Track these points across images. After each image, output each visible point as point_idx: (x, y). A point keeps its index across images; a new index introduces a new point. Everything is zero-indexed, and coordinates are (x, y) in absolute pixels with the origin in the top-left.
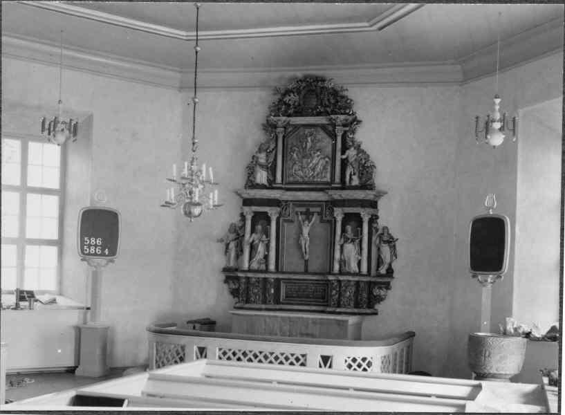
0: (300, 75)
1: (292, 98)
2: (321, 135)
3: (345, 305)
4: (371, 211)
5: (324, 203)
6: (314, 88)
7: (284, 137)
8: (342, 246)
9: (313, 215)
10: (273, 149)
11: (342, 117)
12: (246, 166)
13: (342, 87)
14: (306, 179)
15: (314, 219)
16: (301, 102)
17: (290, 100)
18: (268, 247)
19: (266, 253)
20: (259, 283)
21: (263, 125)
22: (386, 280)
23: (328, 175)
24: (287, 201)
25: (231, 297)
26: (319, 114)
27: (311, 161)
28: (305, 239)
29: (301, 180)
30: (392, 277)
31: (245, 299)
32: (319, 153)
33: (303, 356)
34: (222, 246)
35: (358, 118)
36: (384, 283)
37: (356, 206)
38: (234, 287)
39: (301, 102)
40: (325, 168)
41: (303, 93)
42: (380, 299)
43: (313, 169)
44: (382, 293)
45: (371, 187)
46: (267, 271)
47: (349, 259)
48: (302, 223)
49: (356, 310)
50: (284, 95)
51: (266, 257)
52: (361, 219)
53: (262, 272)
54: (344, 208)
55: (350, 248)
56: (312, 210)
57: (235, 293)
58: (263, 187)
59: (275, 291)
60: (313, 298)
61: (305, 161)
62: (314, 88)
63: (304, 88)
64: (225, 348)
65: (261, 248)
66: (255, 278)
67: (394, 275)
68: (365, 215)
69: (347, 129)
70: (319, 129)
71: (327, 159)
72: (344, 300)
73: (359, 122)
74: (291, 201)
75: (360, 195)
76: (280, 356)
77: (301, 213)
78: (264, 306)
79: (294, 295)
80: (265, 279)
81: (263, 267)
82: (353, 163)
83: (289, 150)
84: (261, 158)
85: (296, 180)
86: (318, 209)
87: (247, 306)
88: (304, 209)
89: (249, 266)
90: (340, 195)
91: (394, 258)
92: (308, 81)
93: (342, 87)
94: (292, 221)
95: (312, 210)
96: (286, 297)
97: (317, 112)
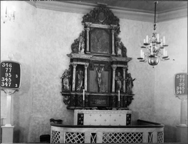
77: (97, 66)
88: (98, 65)
95: (101, 65)
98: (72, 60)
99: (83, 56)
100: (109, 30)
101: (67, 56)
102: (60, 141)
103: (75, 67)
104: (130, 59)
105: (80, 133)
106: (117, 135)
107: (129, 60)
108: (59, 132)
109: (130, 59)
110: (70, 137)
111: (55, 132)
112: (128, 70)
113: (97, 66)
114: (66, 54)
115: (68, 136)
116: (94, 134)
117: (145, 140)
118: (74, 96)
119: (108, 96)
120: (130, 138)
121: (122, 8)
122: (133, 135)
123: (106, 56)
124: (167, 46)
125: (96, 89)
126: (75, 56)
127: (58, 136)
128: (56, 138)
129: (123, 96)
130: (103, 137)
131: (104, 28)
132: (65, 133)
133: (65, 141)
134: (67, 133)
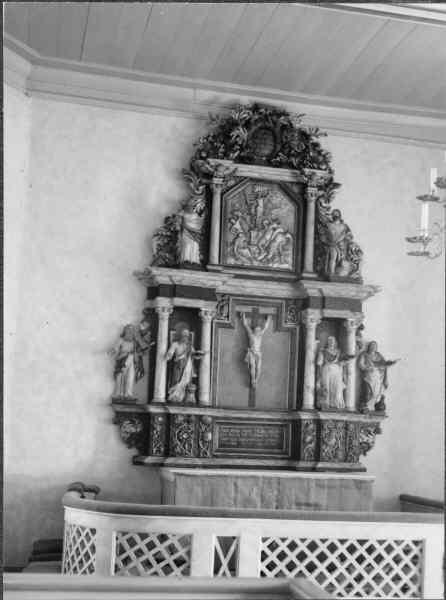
0: (246, 100)
2: (279, 198)
3: (330, 458)
5: (284, 302)
6: (271, 125)
7: (222, 195)
9: (266, 318)
11: (319, 173)
14: (256, 264)
15: (267, 325)
17: (238, 136)
18: (197, 365)
19: (195, 376)
20: (188, 422)
21: (184, 172)
22: (375, 420)
24: (224, 295)
26: (279, 165)
27: (264, 236)
28: (256, 356)
29: (248, 264)
30: (384, 416)
32: (275, 225)
33: (416, 543)
34: (108, 364)
35: (336, 181)
36: (371, 425)
38: (133, 430)
41: (254, 128)
42: (366, 448)
43: (267, 249)
44: (370, 439)
45: (358, 281)
46: (198, 404)
48: (250, 331)
51: (196, 381)
53: (191, 405)
55: (334, 371)
56: (262, 310)
57: (130, 441)
60: (266, 447)
61: (254, 234)
62: (271, 125)
64: (274, 537)
66: (183, 415)
67: (387, 411)
68: (350, 317)
69: (321, 193)
71: (289, 236)
72: (326, 450)
73: (337, 185)
76: (377, 546)
77: (248, 315)
78: (199, 462)
80: (200, 418)
82: (342, 244)
83: (230, 216)
84: (190, 221)
85: (239, 263)
86: (271, 311)
88: (249, 309)
89: (167, 395)
92: (261, 113)
93: (317, 130)
94: (229, 327)
95: (262, 310)
98: (154, 291)
99: (159, 272)
100: (296, 189)
101: (134, 278)
102: (94, 564)
104: (372, 290)
105: (174, 535)
106: (277, 546)
107: (370, 294)
108: (93, 531)
109: (372, 290)
110: (136, 548)
111: (78, 532)
112: (214, 289)
114: (131, 273)
115: (126, 546)
116: (226, 543)
117: (202, 564)
119: (289, 420)
120: (370, 559)
122: (380, 550)
123: (280, 280)
124: (420, 198)
125: (241, 395)
126: (164, 276)
127: (88, 546)
128: (83, 553)
129: (346, 422)
130: (263, 553)
132: (114, 535)
133: (113, 562)
134: (124, 534)
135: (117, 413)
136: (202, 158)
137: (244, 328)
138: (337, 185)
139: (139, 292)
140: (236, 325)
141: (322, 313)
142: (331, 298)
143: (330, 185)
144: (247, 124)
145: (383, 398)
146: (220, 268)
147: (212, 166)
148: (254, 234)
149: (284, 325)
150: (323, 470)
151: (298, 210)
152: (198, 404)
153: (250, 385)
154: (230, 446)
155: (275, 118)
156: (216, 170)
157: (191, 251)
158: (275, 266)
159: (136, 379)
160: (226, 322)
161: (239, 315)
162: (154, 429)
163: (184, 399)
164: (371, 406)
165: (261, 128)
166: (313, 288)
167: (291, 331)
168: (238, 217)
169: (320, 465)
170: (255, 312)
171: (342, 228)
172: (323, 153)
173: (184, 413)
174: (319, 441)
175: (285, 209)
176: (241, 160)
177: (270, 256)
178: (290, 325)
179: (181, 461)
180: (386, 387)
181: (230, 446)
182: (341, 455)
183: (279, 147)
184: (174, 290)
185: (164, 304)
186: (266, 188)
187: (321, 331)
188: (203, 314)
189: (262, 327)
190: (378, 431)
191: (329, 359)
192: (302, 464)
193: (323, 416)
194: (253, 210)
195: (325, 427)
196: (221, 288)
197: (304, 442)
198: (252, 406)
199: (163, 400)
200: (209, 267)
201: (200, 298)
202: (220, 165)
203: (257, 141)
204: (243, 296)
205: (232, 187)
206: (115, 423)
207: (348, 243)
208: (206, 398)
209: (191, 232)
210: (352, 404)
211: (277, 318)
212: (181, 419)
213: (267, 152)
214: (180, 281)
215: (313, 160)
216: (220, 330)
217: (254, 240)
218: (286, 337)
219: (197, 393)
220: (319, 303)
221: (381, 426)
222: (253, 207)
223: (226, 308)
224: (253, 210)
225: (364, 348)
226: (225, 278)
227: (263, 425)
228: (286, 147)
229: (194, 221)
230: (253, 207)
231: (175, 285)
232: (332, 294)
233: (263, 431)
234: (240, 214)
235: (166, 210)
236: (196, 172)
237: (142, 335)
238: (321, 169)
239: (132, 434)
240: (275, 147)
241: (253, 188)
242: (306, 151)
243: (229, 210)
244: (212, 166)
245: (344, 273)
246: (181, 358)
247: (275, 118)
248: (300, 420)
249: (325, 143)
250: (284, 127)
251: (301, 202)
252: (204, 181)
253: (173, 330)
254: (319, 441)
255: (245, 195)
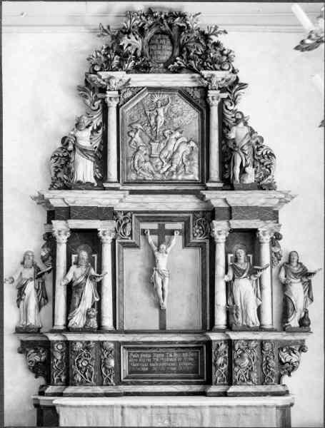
1: (133, 43)
2: (181, 105)
4: (271, 224)
5: (191, 215)
7: (118, 107)
8: (229, 287)
10: (99, 128)
11: (219, 75)
12: (51, 154)
13: (216, 28)
14: (159, 177)
16: (146, 51)
17: (129, 45)
18: (99, 287)
21: (80, 88)
22: (298, 337)
23: (196, 170)
24: (125, 213)
25: (32, 376)
26: (178, 70)
29: (150, 178)
30: (309, 331)
31: (63, 378)
32: (178, 134)
36: (296, 343)
37: (251, 218)
38: (37, 358)
39: (146, 51)
40: (189, 158)
41: (149, 35)
43: (171, 160)
44: (294, 358)
45: (271, 187)
47: (246, 306)
49: (262, 389)
50: (116, 38)
51: (98, 305)
52: (99, 239)
53: (91, 331)
54: (70, 221)
55: (244, 287)
56: (168, 226)
58: (89, 187)
59: (115, 362)
60: (178, 372)
61: (154, 145)
62: (168, 28)
63: (150, 27)
65: (89, 290)
66: (81, 342)
68: (265, 230)
69: (225, 95)
70: (177, 95)
71: (193, 144)
72: (239, 372)
73: (243, 86)
74: (135, 212)
75: (257, 199)
77: (153, 232)
78: (100, 390)
79: (144, 369)
80: (101, 344)
81: (93, 323)
86: (179, 226)
87: (70, 390)
88: (155, 226)
89: (67, 321)
90: (225, 201)
91: (309, 302)
93: (216, 28)
94: (135, 246)
95: (168, 226)
96: (130, 373)
97: (175, 67)
98: (52, 214)
99: (213, 196)
103: (62, 241)
113: (153, 232)
118: (60, 347)
121: (89, 390)
126: (60, 199)
131: (179, 84)
135: (22, 341)
136: (95, 72)
137: (150, 245)
138: (243, 86)
139: (41, 216)
140: (142, 243)
141: (229, 225)
142: (237, 207)
143: (233, 87)
144: (142, 31)
145: (306, 312)
146: (117, 185)
147: (104, 80)
148: (154, 145)
149: (192, 240)
150: (235, 395)
151: (202, 116)
152: (100, 329)
153: (159, 306)
154: (142, 372)
155: (170, 20)
156: (109, 83)
157: (85, 169)
158: (180, 177)
159: (40, 306)
160: (130, 240)
161: (144, 232)
162: (54, 357)
163: (85, 325)
164: (294, 322)
165: (157, 33)
166: (217, 199)
167: (201, 246)
168: (137, 130)
169: (232, 389)
170: (162, 228)
171: (246, 130)
172: (225, 52)
173: (81, 339)
174: (231, 362)
175: (189, 117)
176: (136, 70)
177: (173, 169)
178: (199, 239)
179: (81, 390)
180: (312, 300)
181: (142, 372)
182: (254, 376)
183: (177, 52)
184: (68, 213)
185: (59, 226)
186: (166, 96)
187: (233, 244)
188: (100, 234)
189: (169, 244)
190: (302, 349)
191: (238, 273)
192: (213, 389)
193: (233, 336)
194: (153, 122)
195: (237, 348)
196: (120, 207)
197: (216, 365)
198: (163, 329)
199: (62, 328)
200: (106, 185)
201: (97, 218)
202: (111, 77)
203: (153, 47)
204: (147, 212)
205: (129, 99)
206: (20, 352)
207: (259, 145)
208: (108, 322)
209: (83, 150)
210: (268, 320)
211: (185, 233)
212: (79, 346)
213: (165, 58)
214: (74, 202)
215: (214, 61)
216: (126, 251)
217: (155, 153)
218: (197, 252)
219: (99, 318)
220: (227, 212)
221: (307, 344)
222: (153, 118)
223: (129, 226)
224: (153, 122)
225: (284, 260)
226: (119, 194)
227: (176, 348)
228: (183, 49)
229: (85, 139)
230: (153, 118)
231: (70, 207)
232: (239, 203)
233: (175, 355)
234: (139, 126)
235: (65, 130)
236: (91, 89)
237: (44, 262)
238: (223, 70)
239: (37, 363)
240: (173, 51)
241: (152, 97)
242: (206, 53)
243: (127, 122)
244: (104, 80)
245: (250, 178)
246: (79, 281)
247: (170, 20)
248: (211, 341)
249: (226, 41)
250: (181, 29)
251: (203, 107)
252: (100, 95)
253: (231, 253)
254: (231, 362)
255: (143, 105)
